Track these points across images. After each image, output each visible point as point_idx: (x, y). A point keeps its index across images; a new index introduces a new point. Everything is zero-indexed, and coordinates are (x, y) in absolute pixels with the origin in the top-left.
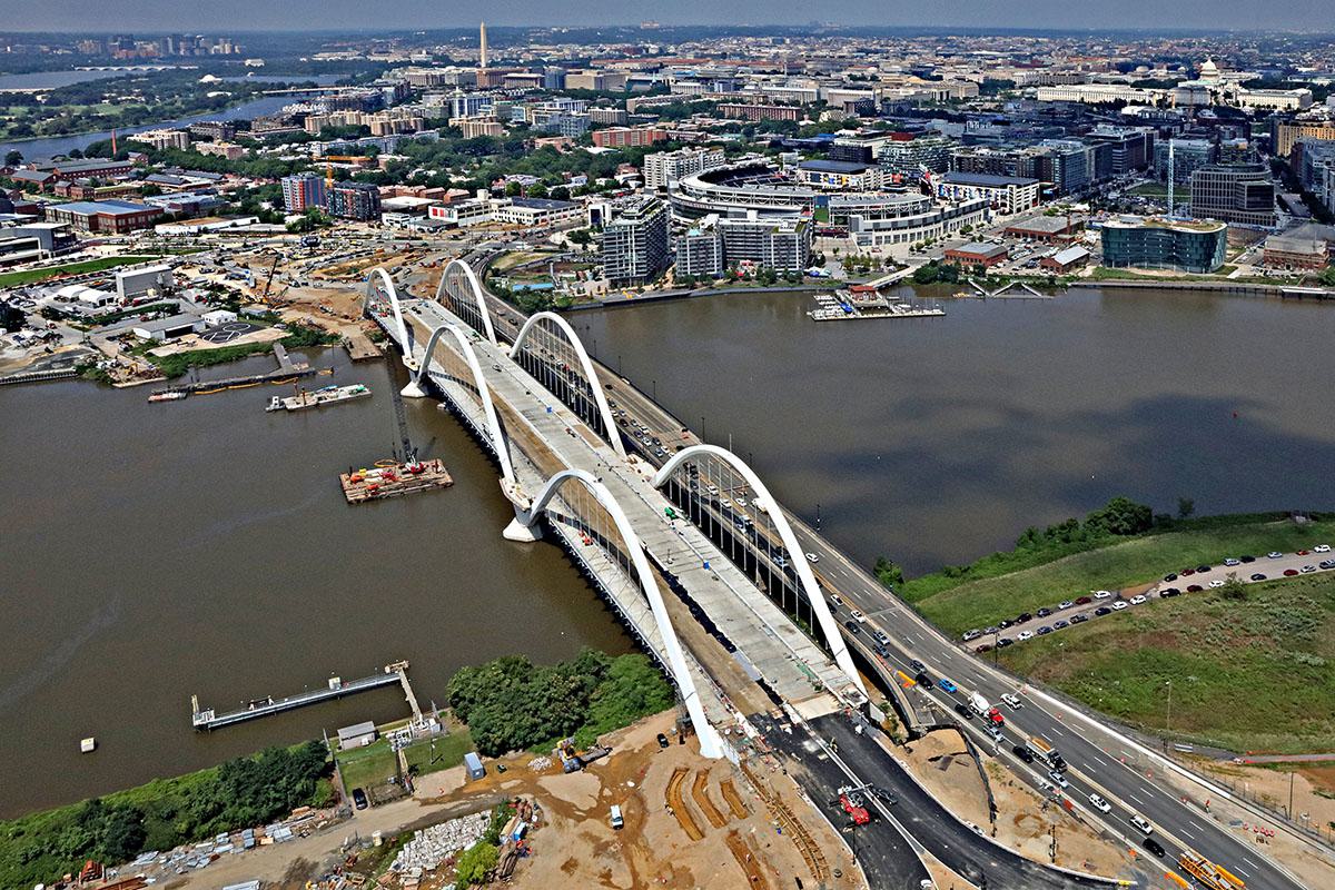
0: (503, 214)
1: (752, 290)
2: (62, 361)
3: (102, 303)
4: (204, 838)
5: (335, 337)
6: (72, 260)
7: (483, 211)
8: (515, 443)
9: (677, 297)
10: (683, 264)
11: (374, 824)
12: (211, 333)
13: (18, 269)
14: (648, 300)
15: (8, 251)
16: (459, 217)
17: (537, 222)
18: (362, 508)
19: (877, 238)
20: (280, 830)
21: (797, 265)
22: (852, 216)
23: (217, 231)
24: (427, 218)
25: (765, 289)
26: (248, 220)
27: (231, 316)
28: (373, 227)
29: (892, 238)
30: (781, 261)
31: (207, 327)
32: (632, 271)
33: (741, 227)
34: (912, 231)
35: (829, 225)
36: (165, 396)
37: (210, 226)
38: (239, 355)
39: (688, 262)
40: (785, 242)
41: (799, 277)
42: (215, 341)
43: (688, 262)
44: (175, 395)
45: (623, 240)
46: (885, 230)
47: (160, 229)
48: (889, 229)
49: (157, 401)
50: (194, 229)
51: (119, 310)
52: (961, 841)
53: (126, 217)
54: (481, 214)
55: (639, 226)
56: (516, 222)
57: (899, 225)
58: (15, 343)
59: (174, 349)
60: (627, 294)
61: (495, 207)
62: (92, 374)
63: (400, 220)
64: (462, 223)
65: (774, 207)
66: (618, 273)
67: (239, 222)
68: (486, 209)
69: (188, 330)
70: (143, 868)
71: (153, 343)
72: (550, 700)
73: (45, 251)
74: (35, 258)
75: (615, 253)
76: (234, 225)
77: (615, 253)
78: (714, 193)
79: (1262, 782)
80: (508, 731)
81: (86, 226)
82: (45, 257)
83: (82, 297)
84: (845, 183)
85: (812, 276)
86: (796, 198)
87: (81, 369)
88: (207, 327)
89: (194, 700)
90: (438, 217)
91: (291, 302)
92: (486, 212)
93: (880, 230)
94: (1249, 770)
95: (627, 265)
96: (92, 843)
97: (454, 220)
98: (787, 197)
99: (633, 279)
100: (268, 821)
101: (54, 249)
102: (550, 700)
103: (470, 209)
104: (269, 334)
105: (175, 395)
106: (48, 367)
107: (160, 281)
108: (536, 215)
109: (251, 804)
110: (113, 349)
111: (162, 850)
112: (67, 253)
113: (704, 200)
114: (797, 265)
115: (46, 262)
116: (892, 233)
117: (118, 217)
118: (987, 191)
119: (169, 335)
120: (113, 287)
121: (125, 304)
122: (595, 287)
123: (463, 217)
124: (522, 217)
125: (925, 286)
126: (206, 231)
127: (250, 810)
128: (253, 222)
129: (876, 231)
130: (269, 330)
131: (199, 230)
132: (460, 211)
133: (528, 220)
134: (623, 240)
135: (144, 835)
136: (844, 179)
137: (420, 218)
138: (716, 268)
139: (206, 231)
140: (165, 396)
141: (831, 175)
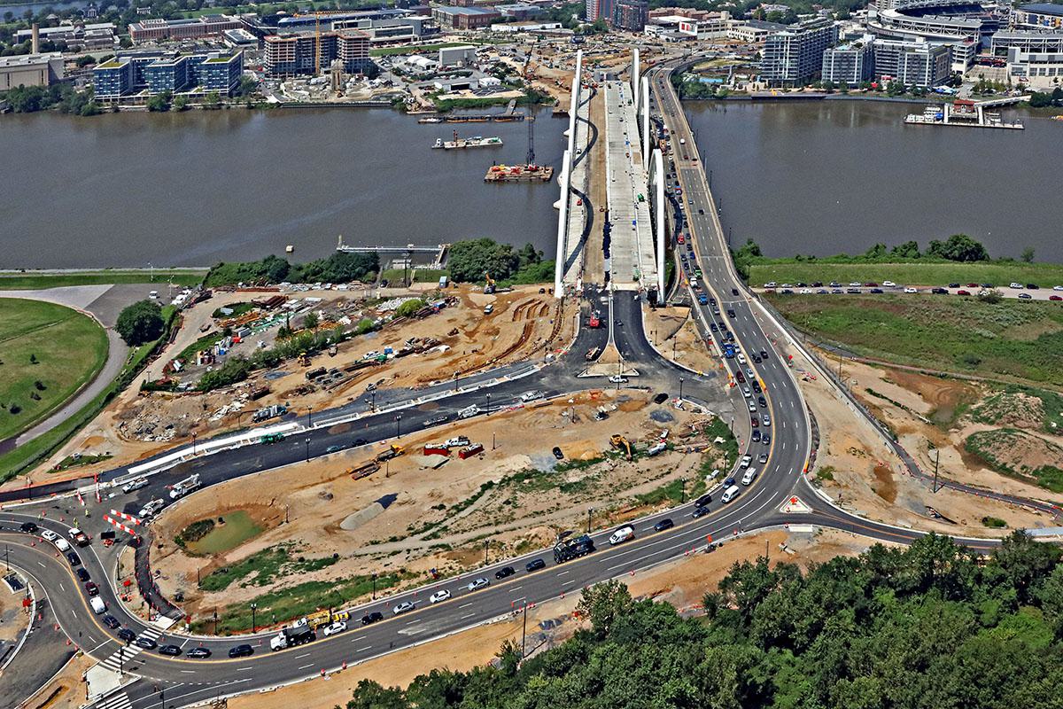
0: (735, 32)
1: (881, 99)
2: (386, 97)
3: (428, 68)
4: (311, 283)
5: (552, 99)
6: (430, 43)
7: (720, 28)
8: (589, 161)
9: (814, 98)
10: (829, 72)
11: (380, 292)
12: (483, 90)
13: (396, 46)
14: (794, 98)
15: (394, 34)
16: (698, 32)
17: (757, 40)
18: (492, 185)
19: (1032, 69)
20: (343, 286)
21: (926, 81)
22: (1012, 47)
23: (529, 31)
24: (678, 31)
25: (891, 99)
26: (554, 25)
27: (497, 81)
28: (636, 36)
29: (1047, 71)
30: (912, 77)
31: (479, 86)
32: (785, 74)
33: (889, 47)
34: (1052, 66)
35: (990, 54)
36: (429, 120)
37: (526, 28)
38: (487, 104)
39: (832, 71)
40: (917, 60)
41: (924, 91)
42: (479, 95)
43: (832, 71)
44: (435, 120)
45: (780, 48)
46: (1041, 62)
47: (494, 27)
48: (1045, 63)
49: (423, 122)
50: (515, 29)
51: (436, 73)
52: (637, 343)
53: (475, 17)
54: (718, 30)
55: (794, 38)
56: (742, 39)
57: (1056, 59)
58: (369, 86)
59: (453, 97)
60: (775, 92)
61: (730, 26)
62: (398, 105)
63: (655, 31)
64: (700, 36)
65: (940, 35)
66: (773, 75)
67: (548, 26)
68: (723, 27)
69: (466, 87)
70: (282, 287)
71: (442, 92)
72: (492, 259)
73: (416, 36)
74: (409, 40)
75: (772, 58)
76: (544, 28)
77: (772, 58)
78: (898, 21)
79: (863, 375)
80: (466, 268)
81: (451, 23)
82: (415, 40)
83: (419, 63)
84: (1058, 25)
85: (938, 93)
86: (963, 28)
87: (395, 102)
88: (479, 86)
89: (340, 237)
90: (685, 31)
91: (541, 77)
92: (723, 30)
93: (1036, 63)
94: (856, 363)
95: (781, 69)
96: (265, 272)
97: (695, 34)
98: (956, 28)
99: (785, 82)
100: (340, 282)
101: (422, 35)
102: (492, 259)
103: (708, 25)
104: (516, 93)
105: (435, 120)
106: (378, 99)
107: (466, 56)
108: (757, 34)
109: (334, 271)
110: (418, 93)
111: (292, 283)
112: (430, 38)
113: (888, 27)
114: (926, 81)
115: (415, 43)
116: (1047, 66)
117: (470, 17)
118: (1041, 18)
119: (453, 88)
120: (437, 59)
121: (441, 70)
122: (755, 87)
123: (702, 31)
124: (747, 35)
125: (1036, 109)
126: (523, 31)
127: (333, 274)
128: (558, 27)
129: (1032, 63)
130: (515, 91)
131: (519, 30)
132: (699, 27)
133: (751, 37)
134: (780, 48)
135: (287, 274)
136: (1058, 21)
137: (672, 31)
138: (855, 79)
139: (523, 31)
140: (429, 120)
141: (1046, 17)
